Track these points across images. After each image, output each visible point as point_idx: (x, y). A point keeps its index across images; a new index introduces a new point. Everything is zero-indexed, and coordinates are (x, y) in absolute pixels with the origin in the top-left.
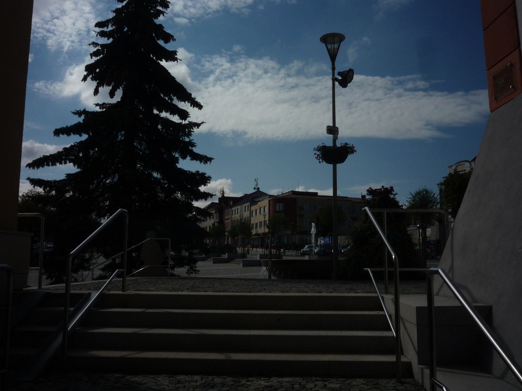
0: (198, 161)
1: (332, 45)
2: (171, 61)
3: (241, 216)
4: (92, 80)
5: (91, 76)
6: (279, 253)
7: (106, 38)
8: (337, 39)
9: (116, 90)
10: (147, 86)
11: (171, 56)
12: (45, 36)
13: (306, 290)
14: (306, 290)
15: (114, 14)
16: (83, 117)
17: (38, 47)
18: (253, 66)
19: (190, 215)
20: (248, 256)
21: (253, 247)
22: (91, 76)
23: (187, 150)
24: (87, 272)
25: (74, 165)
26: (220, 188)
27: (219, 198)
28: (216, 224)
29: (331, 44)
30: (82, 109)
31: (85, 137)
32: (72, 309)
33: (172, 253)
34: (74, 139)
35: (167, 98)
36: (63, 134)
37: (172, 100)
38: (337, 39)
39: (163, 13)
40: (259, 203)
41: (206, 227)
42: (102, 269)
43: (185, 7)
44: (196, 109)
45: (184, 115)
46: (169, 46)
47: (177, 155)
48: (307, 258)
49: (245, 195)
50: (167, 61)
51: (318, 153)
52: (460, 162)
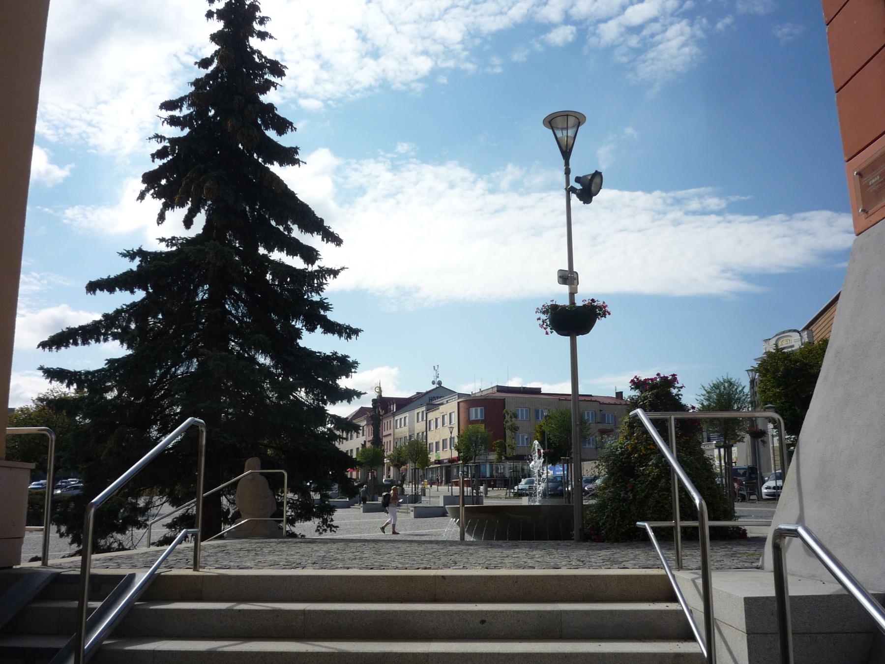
0: (336, 335)
1: (565, 132)
2: (288, 164)
3: (411, 430)
4: (154, 197)
5: (152, 191)
6: (477, 493)
7: (179, 128)
8: (572, 121)
9: (194, 216)
10: (248, 208)
11: (289, 156)
12: (84, 132)
13: (530, 562)
14: (530, 562)
15: (193, 88)
16: (137, 261)
17: (72, 149)
18: (430, 176)
19: (321, 429)
20: (423, 498)
21: (432, 483)
22: (152, 191)
23: (316, 317)
24: (142, 531)
25: (122, 343)
26: (375, 383)
27: (373, 400)
28: (368, 445)
29: (562, 129)
30: (136, 249)
31: (139, 295)
32: (98, 605)
33: (290, 495)
34: (123, 299)
35: (281, 228)
36: (102, 290)
37: (290, 230)
38: (572, 121)
39: (274, 85)
40: (441, 407)
41: (352, 450)
42: (169, 526)
43: (317, 81)
44: (331, 245)
45: (310, 255)
46: (285, 141)
47: (299, 325)
48: (525, 501)
49: (418, 393)
50: (281, 165)
51: (544, 317)
52: (784, 332)
